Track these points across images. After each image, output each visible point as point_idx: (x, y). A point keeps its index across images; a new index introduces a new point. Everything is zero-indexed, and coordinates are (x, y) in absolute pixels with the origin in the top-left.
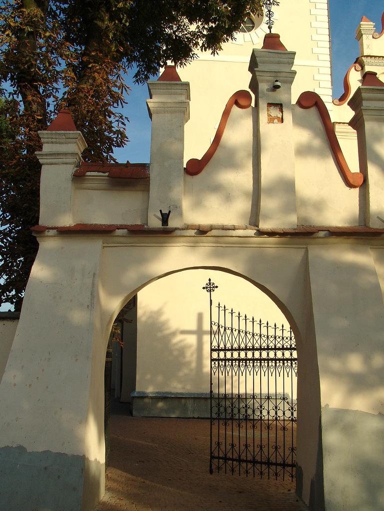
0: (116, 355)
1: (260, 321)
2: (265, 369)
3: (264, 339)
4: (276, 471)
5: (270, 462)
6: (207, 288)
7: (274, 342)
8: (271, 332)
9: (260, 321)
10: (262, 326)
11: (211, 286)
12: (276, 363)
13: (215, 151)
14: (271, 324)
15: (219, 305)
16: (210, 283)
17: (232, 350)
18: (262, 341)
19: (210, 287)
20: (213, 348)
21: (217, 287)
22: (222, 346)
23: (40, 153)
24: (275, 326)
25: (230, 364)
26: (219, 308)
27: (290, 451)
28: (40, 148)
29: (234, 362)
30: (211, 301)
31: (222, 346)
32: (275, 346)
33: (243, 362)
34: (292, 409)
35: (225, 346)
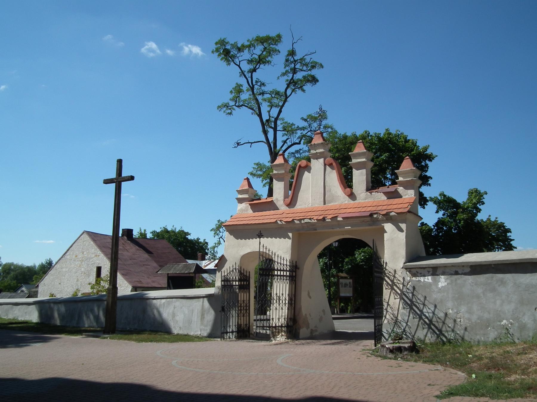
3: (282, 265)
8: (285, 263)
12: (286, 278)
15: (263, 245)
23: (398, 180)
30: (260, 242)
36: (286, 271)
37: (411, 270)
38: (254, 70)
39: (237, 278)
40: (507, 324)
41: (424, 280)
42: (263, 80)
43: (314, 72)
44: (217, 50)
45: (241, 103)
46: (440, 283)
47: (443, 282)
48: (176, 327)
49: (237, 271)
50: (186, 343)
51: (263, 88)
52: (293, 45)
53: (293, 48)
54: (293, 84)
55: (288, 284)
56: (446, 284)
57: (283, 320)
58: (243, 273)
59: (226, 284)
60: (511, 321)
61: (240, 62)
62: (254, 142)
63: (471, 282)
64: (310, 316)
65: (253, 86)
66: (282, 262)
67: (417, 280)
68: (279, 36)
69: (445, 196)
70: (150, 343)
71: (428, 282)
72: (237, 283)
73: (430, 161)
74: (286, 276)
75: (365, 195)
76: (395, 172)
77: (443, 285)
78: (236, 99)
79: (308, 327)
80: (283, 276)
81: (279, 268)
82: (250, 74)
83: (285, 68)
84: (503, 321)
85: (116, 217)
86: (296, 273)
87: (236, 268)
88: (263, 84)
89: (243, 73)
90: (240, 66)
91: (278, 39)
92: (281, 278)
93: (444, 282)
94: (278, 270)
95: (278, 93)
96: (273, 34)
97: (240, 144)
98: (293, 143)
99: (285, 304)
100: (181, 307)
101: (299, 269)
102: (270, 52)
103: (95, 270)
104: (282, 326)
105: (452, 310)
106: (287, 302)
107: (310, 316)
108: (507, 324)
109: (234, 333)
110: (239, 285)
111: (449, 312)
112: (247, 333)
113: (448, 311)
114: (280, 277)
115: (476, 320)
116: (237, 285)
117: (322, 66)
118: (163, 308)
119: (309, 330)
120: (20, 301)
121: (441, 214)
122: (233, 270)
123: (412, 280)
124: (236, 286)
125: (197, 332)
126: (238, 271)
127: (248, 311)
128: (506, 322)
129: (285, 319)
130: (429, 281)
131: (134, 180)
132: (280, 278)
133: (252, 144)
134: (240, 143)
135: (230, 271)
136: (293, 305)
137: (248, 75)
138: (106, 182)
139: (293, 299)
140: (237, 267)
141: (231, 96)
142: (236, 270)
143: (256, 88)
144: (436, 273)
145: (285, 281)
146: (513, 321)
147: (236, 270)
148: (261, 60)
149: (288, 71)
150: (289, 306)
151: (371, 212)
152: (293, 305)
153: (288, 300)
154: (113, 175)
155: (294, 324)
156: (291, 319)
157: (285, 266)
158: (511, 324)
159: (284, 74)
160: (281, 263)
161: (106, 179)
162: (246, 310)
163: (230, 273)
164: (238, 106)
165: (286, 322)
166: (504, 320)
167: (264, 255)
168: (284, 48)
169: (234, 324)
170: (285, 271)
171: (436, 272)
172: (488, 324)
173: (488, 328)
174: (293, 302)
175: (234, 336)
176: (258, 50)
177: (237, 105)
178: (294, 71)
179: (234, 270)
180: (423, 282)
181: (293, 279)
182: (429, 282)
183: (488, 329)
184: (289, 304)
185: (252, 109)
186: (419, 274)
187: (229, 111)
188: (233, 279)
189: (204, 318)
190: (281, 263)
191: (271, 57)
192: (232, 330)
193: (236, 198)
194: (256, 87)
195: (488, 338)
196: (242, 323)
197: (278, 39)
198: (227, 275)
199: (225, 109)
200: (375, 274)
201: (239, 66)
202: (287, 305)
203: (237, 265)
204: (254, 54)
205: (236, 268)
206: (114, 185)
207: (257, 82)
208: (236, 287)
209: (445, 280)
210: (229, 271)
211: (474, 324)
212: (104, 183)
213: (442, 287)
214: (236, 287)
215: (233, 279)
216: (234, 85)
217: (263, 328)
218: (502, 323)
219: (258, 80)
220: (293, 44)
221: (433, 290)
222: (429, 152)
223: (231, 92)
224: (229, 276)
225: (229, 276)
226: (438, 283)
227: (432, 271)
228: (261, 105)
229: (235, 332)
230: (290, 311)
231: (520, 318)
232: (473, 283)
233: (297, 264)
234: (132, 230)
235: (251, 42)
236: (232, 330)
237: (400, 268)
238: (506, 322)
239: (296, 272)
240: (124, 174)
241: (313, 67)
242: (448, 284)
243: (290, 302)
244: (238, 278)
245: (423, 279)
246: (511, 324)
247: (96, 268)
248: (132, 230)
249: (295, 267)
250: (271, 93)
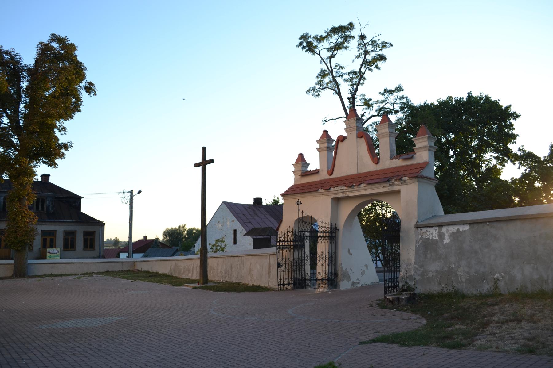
0: (14, 234)
2: (322, 241)
3: (322, 228)
6: (297, 203)
8: (324, 225)
12: (326, 238)
14: (324, 222)
16: (299, 201)
17: (323, 232)
18: (321, 229)
19: (299, 203)
21: (302, 203)
22: (306, 230)
23: (415, 147)
28: (414, 145)
30: (299, 209)
31: (304, 230)
32: (326, 231)
34: (308, 256)
36: (326, 232)
37: (421, 229)
38: (332, 57)
39: (292, 239)
41: (432, 238)
42: (342, 65)
43: (385, 52)
44: (301, 44)
45: (325, 86)
46: (445, 240)
50: (251, 292)
51: (341, 70)
52: (361, 30)
53: (361, 33)
54: (367, 64)
57: (324, 274)
58: (297, 234)
59: (290, 244)
60: (503, 274)
61: (319, 51)
62: (337, 118)
64: (351, 270)
65: (332, 70)
68: (351, 24)
69: (524, 151)
73: (515, 119)
74: (326, 237)
75: (389, 162)
77: (448, 242)
78: (320, 82)
79: (349, 279)
82: (329, 60)
83: (359, 51)
87: (290, 231)
88: (342, 68)
89: (322, 60)
90: (320, 54)
91: (351, 26)
94: (320, 232)
95: (355, 73)
96: (345, 24)
99: (326, 261)
102: (346, 38)
103: (232, 232)
104: (323, 279)
105: (454, 264)
106: (327, 259)
107: (351, 270)
114: (320, 238)
115: (473, 273)
116: (292, 245)
117: (391, 45)
118: (172, 269)
119: (350, 283)
121: (523, 169)
122: (287, 233)
125: (266, 284)
126: (293, 233)
128: (498, 275)
129: (326, 273)
130: (436, 238)
132: (320, 238)
133: (336, 120)
135: (285, 234)
136: (334, 262)
137: (327, 62)
138: (196, 166)
139: (334, 256)
140: (291, 230)
141: (317, 80)
143: (335, 71)
146: (505, 274)
148: (338, 47)
149: (362, 53)
150: (330, 262)
151: (360, 182)
152: (334, 261)
155: (335, 278)
156: (332, 273)
157: (324, 228)
158: (503, 277)
159: (358, 56)
162: (302, 266)
163: (285, 235)
164: (323, 89)
167: (303, 220)
168: (355, 33)
169: (290, 277)
170: (324, 232)
171: (442, 230)
173: (483, 281)
175: (290, 287)
176: (334, 39)
177: (321, 88)
178: (367, 52)
179: (289, 233)
180: (431, 239)
181: (333, 239)
184: (330, 261)
187: (317, 94)
188: (285, 240)
191: (348, 43)
192: (289, 282)
193: (292, 171)
194: (335, 70)
195: (483, 290)
197: (351, 26)
199: (312, 92)
201: (319, 55)
202: (328, 261)
203: (291, 228)
204: (331, 42)
205: (290, 231)
206: (200, 167)
207: (336, 66)
208: (291, 247)
209: (449, 237)
210: (283, 234)
212: (195, 166)
213: (447, 243)
214: (291, 247)
215: (285, 240)
216: (319, 71)
217: (323, 281)
218: (495, 276)
219: (337, 65)
220: (361, 29)
221: (439, 247)
222: (513, 110)
223: (317, 77)
225: (287, 237)
227: (439, 229)
228: (339, 86)
229: (292, 284)
230: (330, 267)
233: (336, 226)
235: (328, 33)
236: (289, 282)
238: (498, 275)
239: (335, 233)
241: (384, 47)
242: (451, 241)
243: (330, 259)
246: (503, 277)
248: (261, 199)
249: (335, 229)
250: (349, 74)
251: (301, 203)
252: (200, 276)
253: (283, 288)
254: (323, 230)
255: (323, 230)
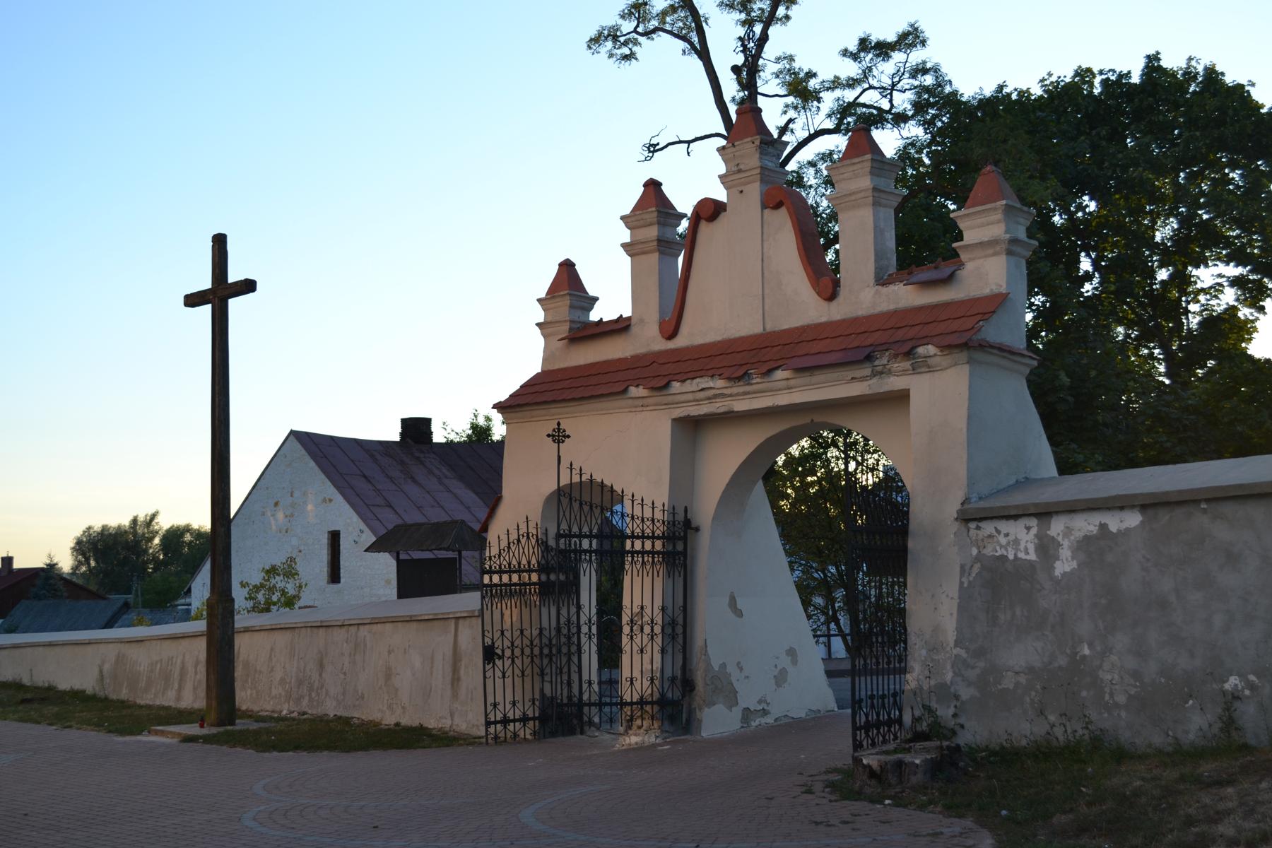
1: (633, 496)
2: (638, 566)
3: (638, 522)
4: (505, 731)
5: (624, 701)
6: (553, 436)
7: (645, 527)
8: (648, 514)
9: (633, 496)
10: (635, 503)
11: (561, 434)
12: (653, 558)
13: (970, 387)
14: (648, 501)
15: (571, 465)
16: (559, 429)
17: (643, 537)
18: (635, 526)
20: (562, 532)
22: (585, 530)
24: (653, 504)
25: (588, 558)
26: (571, 470)
27: (649, 682)
29: (656, 556)
30: (559, 457)
33: (648, 556)
35: (580, 530)
36: (653, 537)
37: (980, 524)
39: (534, 561)
40: (1240, 687)
41: (1015, 555)
45: (654, 23)
46: (1058, 564)
47: (1067, 559)
48: (394, 707)
49: (533, 541)
55: (658, 576)
56: (1074, 564)
57: (646, 683)
60: (1252, 678)
62: (693, 138)
63: (1144, 557)
64: (741, 669)
66: (638, 512)
67: (997, 554)
70: (291, 753)
71: (1026, 560)
72: (535, 577)
74: (652, 553)
76: (952, 219)
77: (1068, 569)
80: (643, 553)
81: (648, 531)
84: (1227, 681)
85: (217, 399)
86: (685, 544)
87: (528, 534)
92: (635, 559)
93: (1070, 559)
94: (633, 537)
97: (657, 147)
98: (812, 132)
100: (405, 649)
101: (697, 529)
105: (1091, 645)
106: (658, 629)
107: (741, 669)
108: (1240, 687)
109: (531, 723)
110: (540, 583)
111: (1080, 654)
112: (575, 722)
113: (1078, 650)
114: (633, 557)
116: (534, 584)
120: (35, 641)
122: (519, 541)
123: (984, 554)
124: (488, 589)
125: (444, 721)
127: (575, 659)
128: (1237, 682)
129: (652, 679)
130: (1028, 557)
131: (183, 296)
132: (633, 559)
133: (691, 144)
134: (658, 144)
135: (509, 544)
136: (680, 640)
138: (189, 303)
139: (680, 620)
142: (528, 538)
144: (1048, 532)
145: (648, 567)
146: (1258, 678)
147: (528, 538)
152: (681, 637)
153: (660, 622)
154: (206, 284)
157: (648, 523)
158: (1252, 687)
160: (632, 515)
161: (189, 292)
162: (569, 654)
163: (509, 548)
165: (655, 689)
166: (1231, 675)
167: (573, 496)
169: (528, 696)
170: (648, 538)
172: (1186, 689)
173: (1188, 703)
174: (679, 630)
175: (528, 731)
179: (523, 541)
182: (1030, 560)
183: (1187, 705)
185: (684, 38)
186: (1002, 535)
189: (459, 679)
190: (632, 515)
195: (1187, 732)
196: (863, 679)
198: (500, 555)
199: (609, 44)
200: (1167, 517)
202: (659, 640)
205: (528, 534)
206: (207, 309)
208: (530, 590)
209: (1072, 552)
210: (504, 544)
211: (1150, 689)
213: (1065, 574)
224: (507, 558)
225: (507, 558)
226: (1054, 562)
228: (704, 24)
229: (534, 719)
230: (669, 658)
231: (1112, 680)
232: (1148, 560)
234: (427, 422)
237: (953, 518)
238: (1237, 682)
240: (234, 276)
242: (1079, 565)
244: (538, 562)
245: (1013, 552)
246: (1252, 687)
247: (326, 535)
248: (427, 422)
251: (564, 436)
252: (208, 697)
253: (502, 735)
254: (643, 532)
255: (643, 532)
